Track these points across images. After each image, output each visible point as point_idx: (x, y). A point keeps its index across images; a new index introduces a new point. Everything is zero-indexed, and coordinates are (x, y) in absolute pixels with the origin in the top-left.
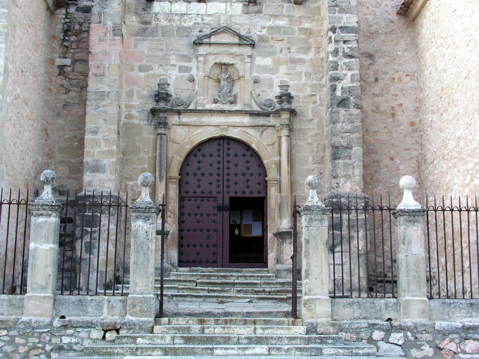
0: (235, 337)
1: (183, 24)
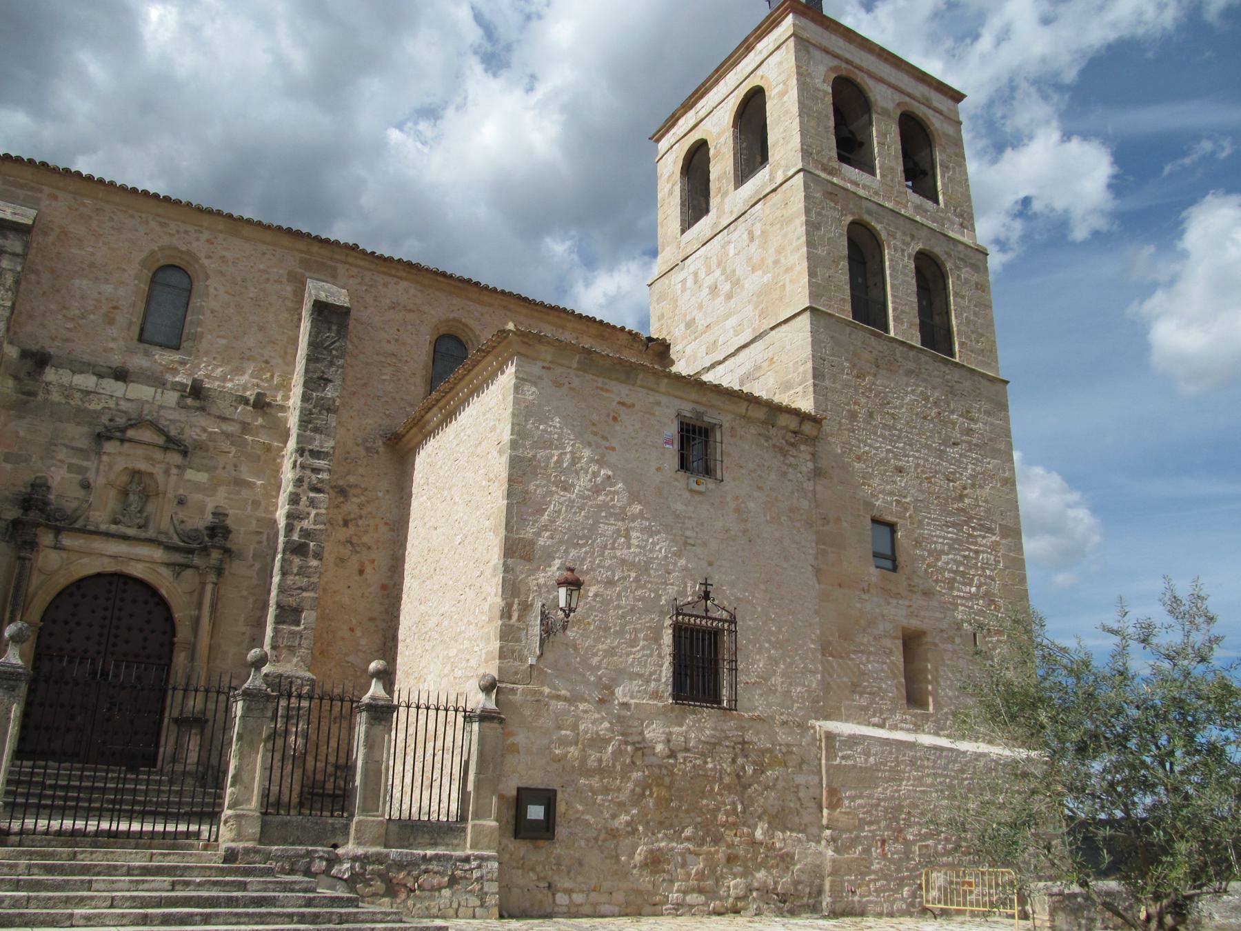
0: (123, 866)
1: (86, 405)
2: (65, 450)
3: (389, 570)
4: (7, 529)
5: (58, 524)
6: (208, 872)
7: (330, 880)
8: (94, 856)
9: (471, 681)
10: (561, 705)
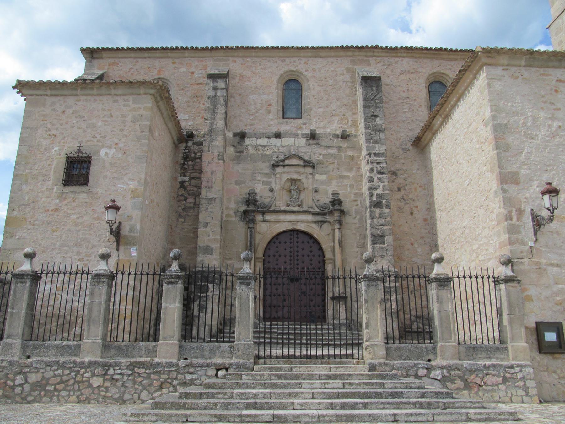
0: (316, 374)
1: (265, 152)
3: (427, 210)
4: (242, 216)
5: (263, 210)
6: (361, 377)
7: (430, 380)
8: (301, 369)
9: (491, 261)
10: (555, 270)
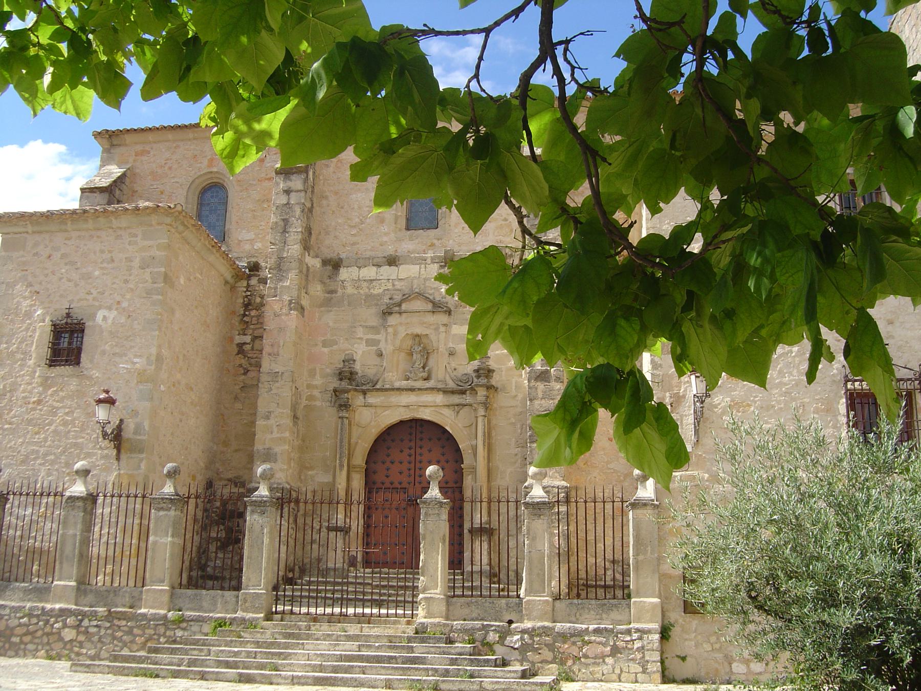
1: (372, 291)
2: (361, 329)
